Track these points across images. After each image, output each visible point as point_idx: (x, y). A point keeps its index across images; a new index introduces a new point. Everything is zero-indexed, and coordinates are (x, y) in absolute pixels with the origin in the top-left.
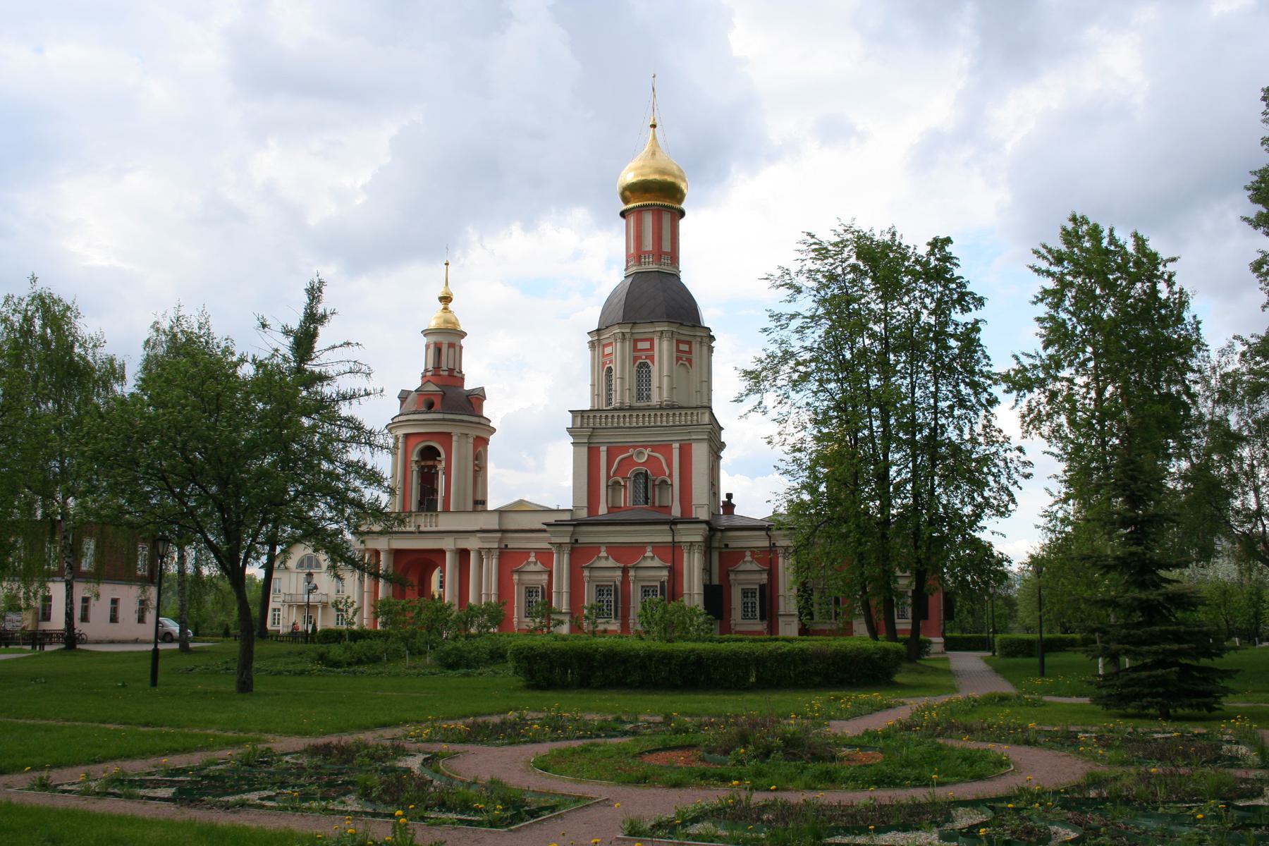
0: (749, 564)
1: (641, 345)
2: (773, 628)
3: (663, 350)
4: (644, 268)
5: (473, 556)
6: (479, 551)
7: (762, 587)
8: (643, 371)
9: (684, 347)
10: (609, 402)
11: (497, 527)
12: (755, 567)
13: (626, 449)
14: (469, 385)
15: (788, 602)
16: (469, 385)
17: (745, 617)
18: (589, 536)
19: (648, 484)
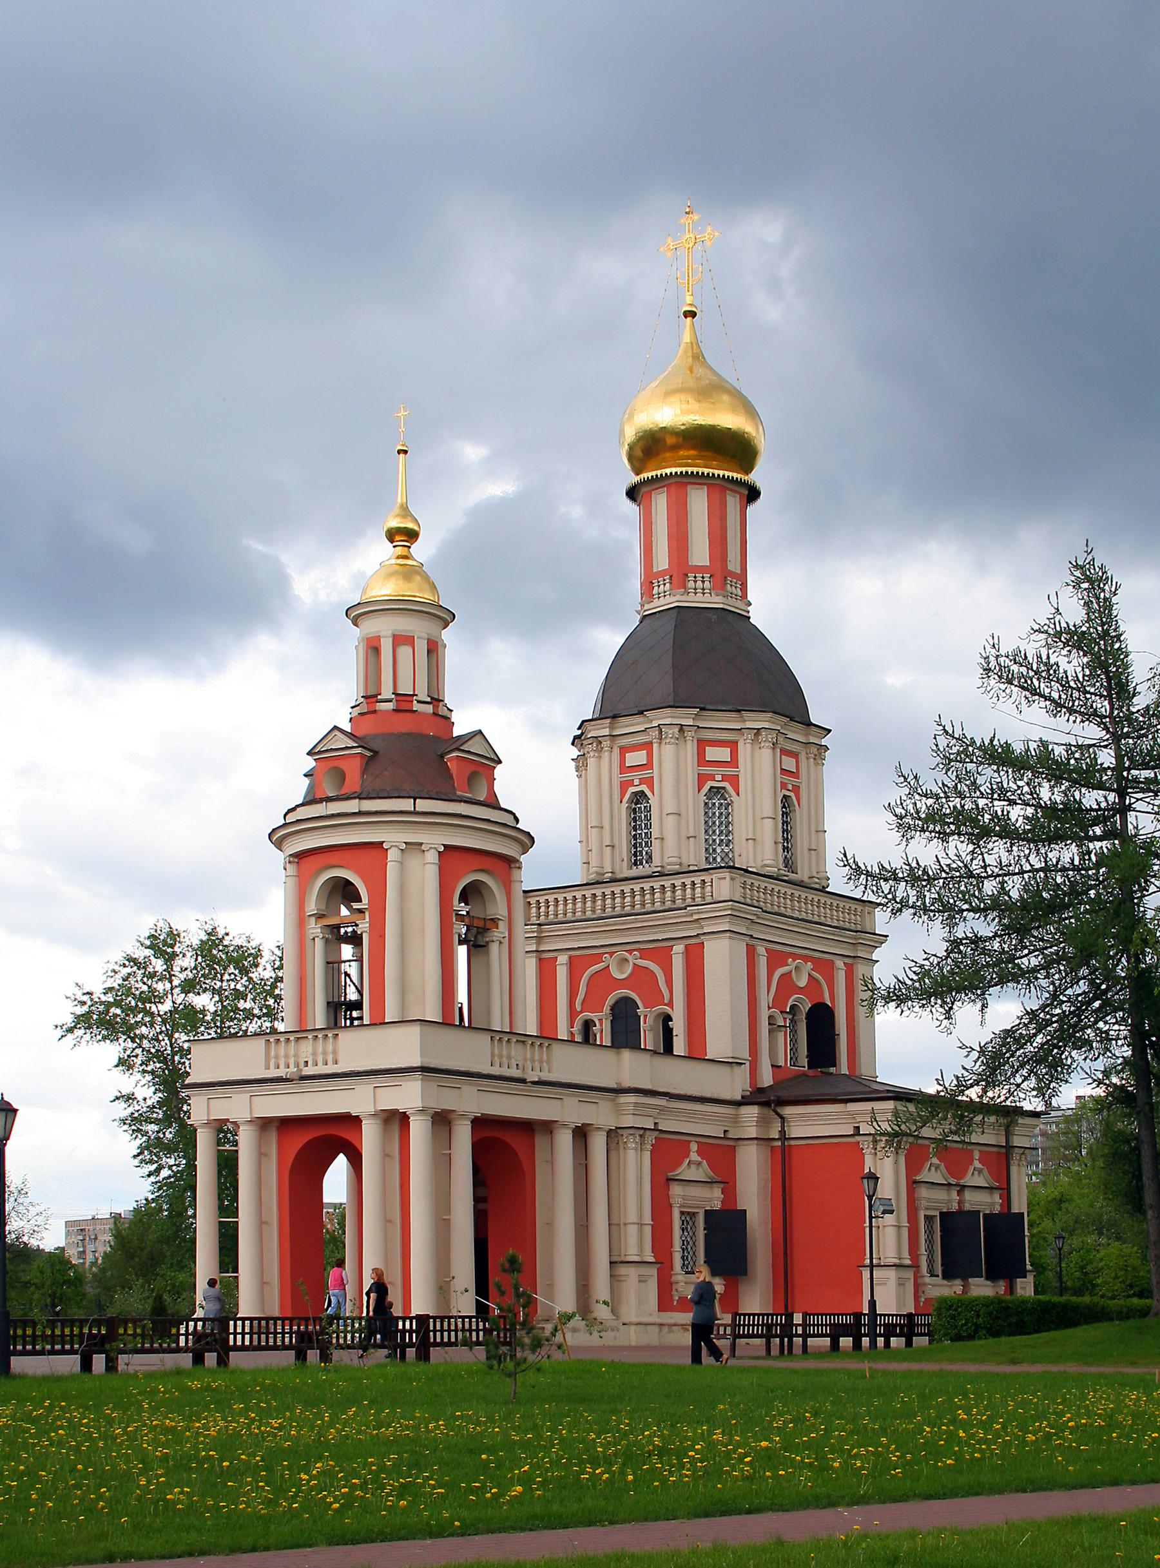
0: (694, 1168)
1: (712, 753)
6: (613, 1135)
8: (717, 798)
9: (789, 764)
10: (639, 852)
11: (416, 1062)
13: (598, 958)
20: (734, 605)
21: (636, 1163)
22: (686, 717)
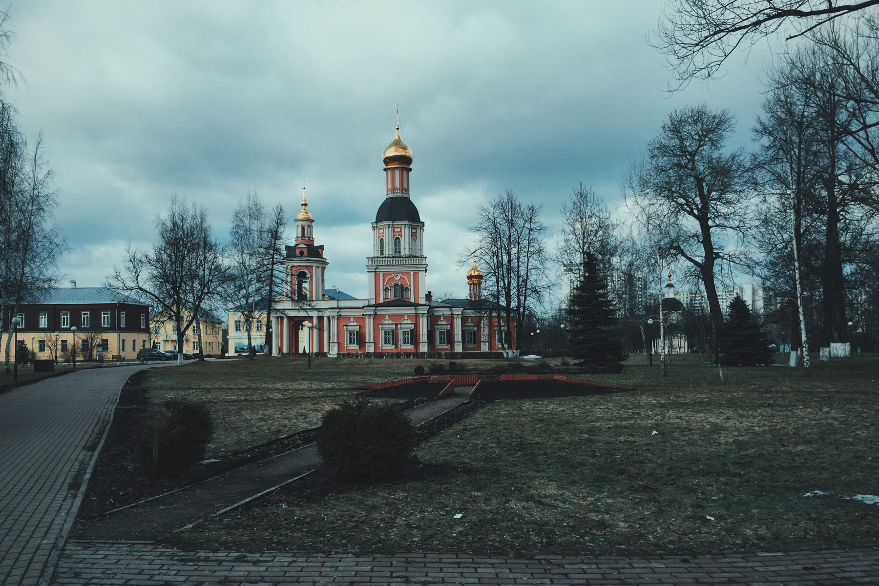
2: (452, 347)
3: (406, 232)
4: (395, 195)
5: (326, 320)
6: (329, 317)
7: (448, 331)
8: (397, 241)
9: (414, 231)
10: (382, 253)
12: (445, 323)
14: (316, 244)
15: (458, 337)
16: (316, 244)
17: (441, 343)
18: (381, 311)
19: (402, 289)
20: (406, 196)
21: (334, 323)
22: (390, 223)
